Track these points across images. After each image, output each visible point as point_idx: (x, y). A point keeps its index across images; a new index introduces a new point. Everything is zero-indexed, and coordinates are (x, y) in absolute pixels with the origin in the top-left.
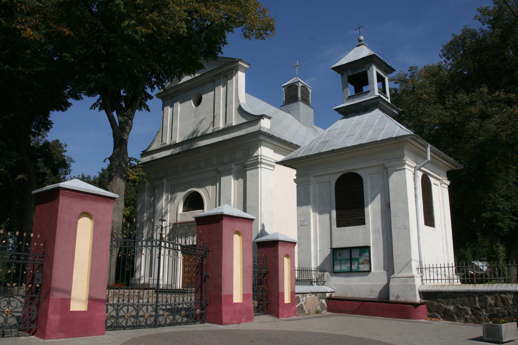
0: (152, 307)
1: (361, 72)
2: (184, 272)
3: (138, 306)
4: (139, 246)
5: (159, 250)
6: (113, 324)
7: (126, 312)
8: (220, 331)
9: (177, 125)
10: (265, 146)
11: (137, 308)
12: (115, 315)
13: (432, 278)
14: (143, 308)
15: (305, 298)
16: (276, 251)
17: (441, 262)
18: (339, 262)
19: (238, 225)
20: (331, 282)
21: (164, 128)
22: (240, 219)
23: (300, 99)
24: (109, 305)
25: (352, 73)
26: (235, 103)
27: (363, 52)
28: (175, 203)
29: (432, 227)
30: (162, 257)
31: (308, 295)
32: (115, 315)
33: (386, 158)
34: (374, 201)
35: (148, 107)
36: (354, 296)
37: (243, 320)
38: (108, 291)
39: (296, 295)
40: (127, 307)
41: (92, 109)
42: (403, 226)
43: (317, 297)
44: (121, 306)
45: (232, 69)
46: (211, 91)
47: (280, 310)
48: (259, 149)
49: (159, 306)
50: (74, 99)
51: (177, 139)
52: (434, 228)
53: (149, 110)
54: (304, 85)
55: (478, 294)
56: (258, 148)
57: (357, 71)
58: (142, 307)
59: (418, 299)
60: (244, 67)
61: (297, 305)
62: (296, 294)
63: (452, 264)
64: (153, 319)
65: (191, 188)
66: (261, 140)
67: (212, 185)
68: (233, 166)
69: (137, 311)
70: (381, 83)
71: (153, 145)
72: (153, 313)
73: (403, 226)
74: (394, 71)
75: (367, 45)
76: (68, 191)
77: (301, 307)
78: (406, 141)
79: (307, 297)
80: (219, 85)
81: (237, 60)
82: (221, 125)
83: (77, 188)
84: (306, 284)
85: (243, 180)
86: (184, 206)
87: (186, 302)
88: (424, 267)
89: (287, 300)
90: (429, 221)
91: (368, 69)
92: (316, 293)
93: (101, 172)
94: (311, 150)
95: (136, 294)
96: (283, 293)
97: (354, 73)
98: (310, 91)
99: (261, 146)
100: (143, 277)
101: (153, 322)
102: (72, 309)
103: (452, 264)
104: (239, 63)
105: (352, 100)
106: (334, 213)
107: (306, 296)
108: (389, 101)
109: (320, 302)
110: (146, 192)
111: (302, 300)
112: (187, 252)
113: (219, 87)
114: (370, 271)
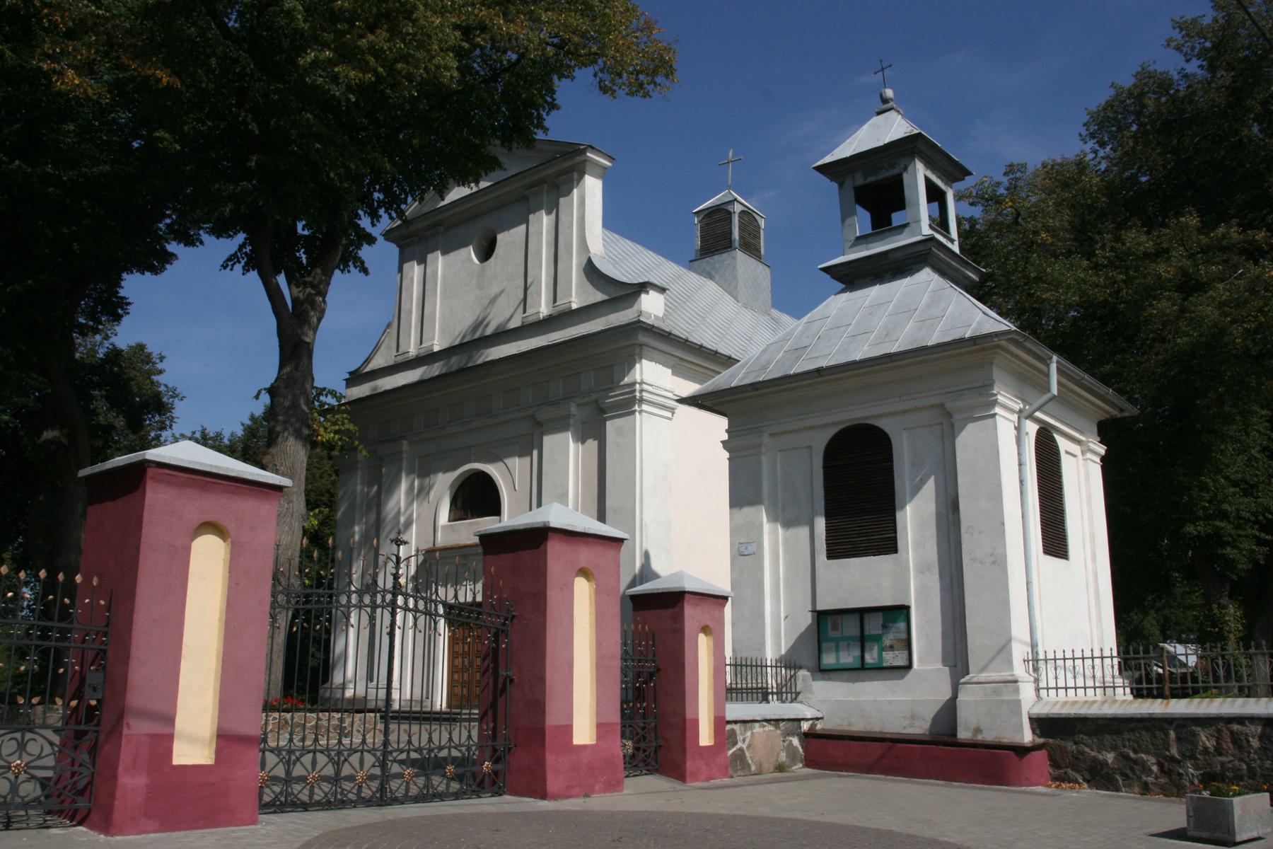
0: (374, 755)
1: (888, 178)
2: (453, 670)
3: (339, 753)
4: (342, 606)
5: (390, 615)
6: (276, 796)
7: (310, 768)
8: (542, 815)
9: (435, 308)
10: (651, 360)
11: (336, 758)
12: (282, 775)
13: (1061, 684)
14: (351, 759)
15: (749, 734)
16: (679, 619)
17: (1083, 645)
18: (833, 644)
19: (585, 554)
20: (813, 693)
21: (402, 316)
22: (590, 540)
23: (737, 244)
24: (268, 750)
25: (865, 179)
26: (579, 253)
27: (893, 127)
28: (431, 498)
29: (1061, 558)
30: (398, 633)
31: (757, 727)
32: (282, 775)
33: (949, 390)
34: (919, 495)
35: (363, 263)
36: (869, 728)
37: (597, 787)
38: (267, 716)
39: (728, 727)
40: (311, 755)
41: (225, 268)
42: (992, 555)
43: (778, 732)
44: (298, 754)
45: (570, 170)
46: (520, 224)
47: (689, 764)
48: (638, 366)
49: (391, 753)
50: (182, 245)
51: (436, 342)
52: (1066, 561)
53: (365, 271)
54: (746, 209)
55: (1175, 723)
56: (634, 365)
57: (876, 175)
58: (349, 755)
59: (1028, 737)
60: (600, 166)
61: (731, 752)
62: (729, 722)
63: (1111, 650)
64: (375, 785)
65: (470, 462)
66: (641, 345)
67: (521, 455)
68: (573, 409)
69: (338, 764)
70: (936, 204)
71: (376, 356)
72: (377, 771)
73: (992, 555)
74: (969, 173)
75: (902, 112)
76: (167, 471)
77: (740, 755)
78: (999, 347)
79: (754, 731)
80: (539, 208)
81: (582, 147)
82: (544, 309)
83: (190, 462)
84: (752, 700)
85: (596, 442)
86: (453, 507)
87: (457, 743)
88: (1041, 656)
89: (706, 738)
90: (1055, 543)
91: (905, 169)
92: (776, 722)
93: (248, 422)
94: (764, 368)
95: (335, 722)
96: (696, 722)
97: (871, 179)
98: (762, 223)
99: (641, 359)
100: (350, 682)
101: (377, 791)
102: (176, 761)
103: (1111, 650)
104: (588, 154)
105: (864, 246)
106: (821, 524)
107: (752, 729)
108: (955, 248)
109: (785, 744)
110: (359, 473)
111: (742, 738)
112: (460, 619)
113: (537, 213)
114: (909, 666)
